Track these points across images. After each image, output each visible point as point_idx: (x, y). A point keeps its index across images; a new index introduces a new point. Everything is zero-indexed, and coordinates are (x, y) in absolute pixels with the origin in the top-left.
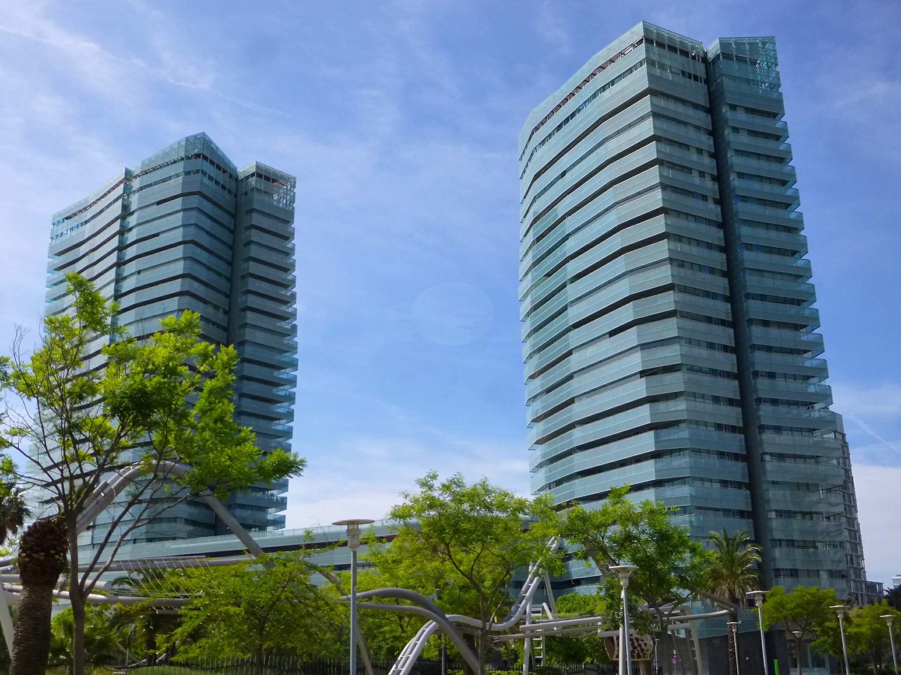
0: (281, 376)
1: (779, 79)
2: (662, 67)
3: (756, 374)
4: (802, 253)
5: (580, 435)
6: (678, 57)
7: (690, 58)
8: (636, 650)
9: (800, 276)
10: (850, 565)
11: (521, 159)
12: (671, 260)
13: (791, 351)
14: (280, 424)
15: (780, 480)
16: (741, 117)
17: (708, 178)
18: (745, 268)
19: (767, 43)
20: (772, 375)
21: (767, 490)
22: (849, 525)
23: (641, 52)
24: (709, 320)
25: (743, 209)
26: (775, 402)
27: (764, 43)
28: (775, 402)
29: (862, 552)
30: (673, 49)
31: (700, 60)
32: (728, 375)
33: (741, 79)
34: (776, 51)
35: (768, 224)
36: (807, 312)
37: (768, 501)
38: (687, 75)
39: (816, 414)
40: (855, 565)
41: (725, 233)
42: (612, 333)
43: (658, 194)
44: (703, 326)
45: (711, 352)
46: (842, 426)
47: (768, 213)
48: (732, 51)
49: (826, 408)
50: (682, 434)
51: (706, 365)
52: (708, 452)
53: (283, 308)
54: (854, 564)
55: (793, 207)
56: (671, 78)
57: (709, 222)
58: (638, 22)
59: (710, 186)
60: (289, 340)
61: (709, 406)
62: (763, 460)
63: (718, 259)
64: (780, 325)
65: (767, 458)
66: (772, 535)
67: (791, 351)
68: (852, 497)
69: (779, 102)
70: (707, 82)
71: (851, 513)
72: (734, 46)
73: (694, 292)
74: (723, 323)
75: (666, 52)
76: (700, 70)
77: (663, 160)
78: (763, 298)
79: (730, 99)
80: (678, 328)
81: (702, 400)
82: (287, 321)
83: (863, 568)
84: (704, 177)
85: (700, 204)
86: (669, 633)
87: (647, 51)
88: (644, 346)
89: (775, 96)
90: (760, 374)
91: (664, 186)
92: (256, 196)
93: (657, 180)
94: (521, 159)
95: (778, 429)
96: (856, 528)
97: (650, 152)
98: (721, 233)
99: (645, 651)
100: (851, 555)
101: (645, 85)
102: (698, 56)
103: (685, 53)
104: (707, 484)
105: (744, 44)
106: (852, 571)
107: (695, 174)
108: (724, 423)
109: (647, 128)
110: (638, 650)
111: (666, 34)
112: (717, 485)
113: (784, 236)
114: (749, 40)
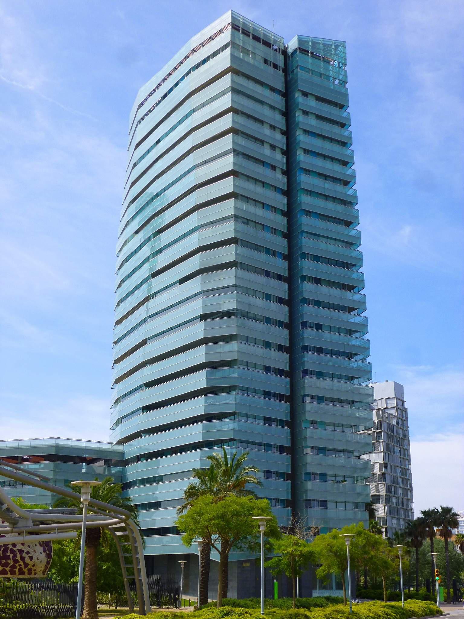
1: (346, 77)
2: (246, 51)
3: (304, 324)
4: (355, 224)
6: (260, 46)
8: (17, 565)
9: (352, 244)
10: (401, 506)
12: (236, 217)
13: (339, 308)
15: (318, 420)
16: (312, 103)
17: (278, 151)
18: (302, 232)
19: (339, 46)
20: (319, 327)
21: (306, 428)
22: (403, 474)
23: (226, 37)
24: (267, 274)
25: (304, 180)
26: (319, 350)
27: (337, 47)
28: (319, 350)
29: (411, 496)
30: (256, 38)
31: (281, 52)
32: (280, 324)
33: (313, 72)
34: (346, 53)
35: (326, 196)
36: (355, 276)
37: (305, 438)
38: (269, 63)
39: (355, 365)
40: (405, 507)
42: (182, 281)
43: (230, 159)
44: (261, 279)
45: (267, 302)
46: (403, 394)
47: (328, 187)
48: (308, 48)
49: (365, 359)
50: (233, 373)
51: (260, 313)
52: (255, 391)
54: (404, 506)
55: (350, 184)
56: (252, 62)
57: (276, 189)
58: (228, 10)
59: (279, 158)
61: (260, 351)
62: (303, 402)
63: (281, 222)
64: (331, 284)
65: (308, 399)
66: (306, 470)
67: (339, 308)
68: (406, 452)
69: (345, 95)
70: (285, 71)
71: (405, 465)
72: (310, 44)
73: (257, 248)
74: (280, 278)
75: (251, 40)
76: (280, 60)
77: (238, 130)
78: (317, 258)
79: (302, 86)
80: (236, 277)
81: (254, 344)
83: (411, 510)
84: (275, 150)
85: (268, 172)
86: (413, 582)
87: (232, 35)
88: (204, 293)
90: (308, 324)
91: (235, 151)
93: (230, 146)
95: (320, 375)
96: (408, 477)
97: (227, 122)
98: (285, 200)
99: (29, 567)
100: (403, 499)
101: (227, 64)
102: (279, 49)
103: (267, 44)
105: (319, 43)
106: (402, 511)
107: (267, 147)
108: (273, 366)
109: (226, 101)
110: (20, 565)
111: (251, 24)
112: (261, 422)
113: (340, 207)
114: (323, 41)
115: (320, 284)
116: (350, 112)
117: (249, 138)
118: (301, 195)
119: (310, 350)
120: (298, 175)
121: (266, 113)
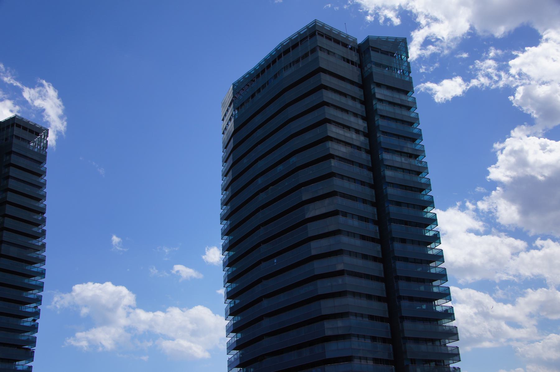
0: (29, 296)
5: (267, 305)
6: (340, 47)
7: (349, 49)
11: (223, 120)
14: (27, 321)
41: (373, 174)
53: (35, 229)
60: (38, 254)
79: (376, 79)
82: (38, 240)
89: (407, 79)
92: (15, 141)
94: (223, 120)
98: (378, 247)
103: (345, 45)
104: (363, 362)
112: (371, 363)
115: (401, 206)
116: (421, 129)
117: (339, 126)
118: (386, 188)
119: (404, 299)
120: (380, 153)
121: (349, 103)
